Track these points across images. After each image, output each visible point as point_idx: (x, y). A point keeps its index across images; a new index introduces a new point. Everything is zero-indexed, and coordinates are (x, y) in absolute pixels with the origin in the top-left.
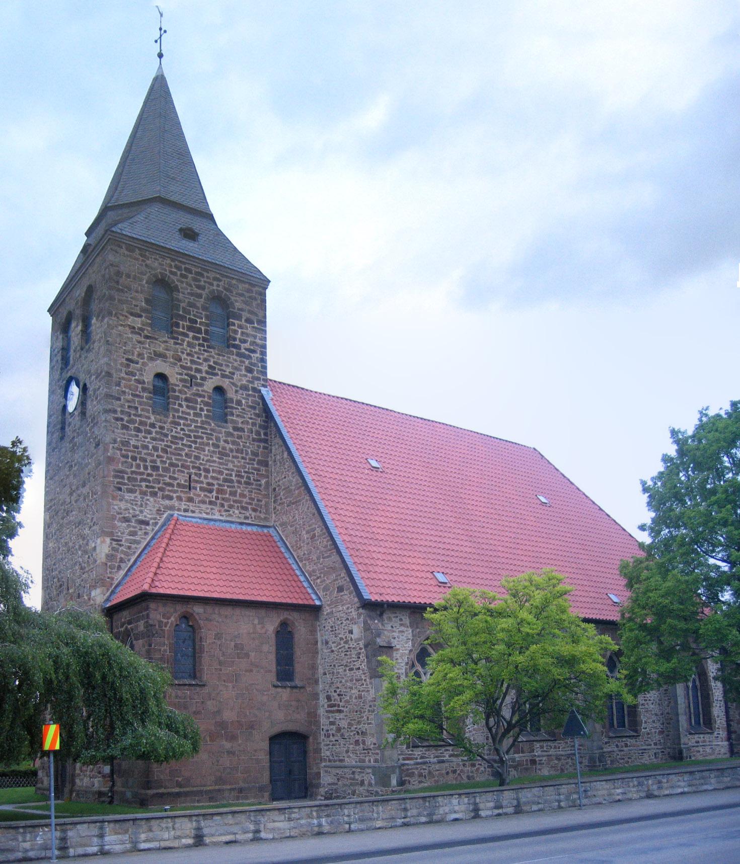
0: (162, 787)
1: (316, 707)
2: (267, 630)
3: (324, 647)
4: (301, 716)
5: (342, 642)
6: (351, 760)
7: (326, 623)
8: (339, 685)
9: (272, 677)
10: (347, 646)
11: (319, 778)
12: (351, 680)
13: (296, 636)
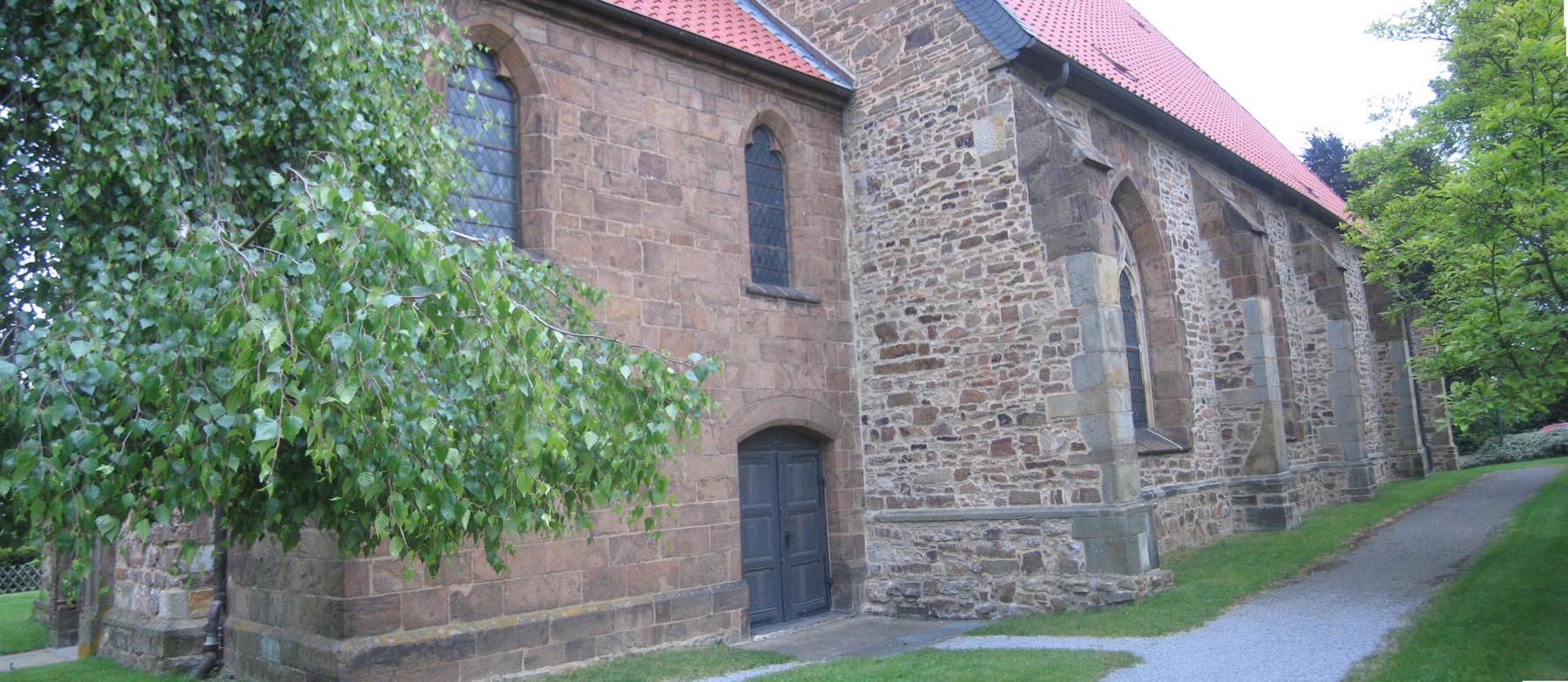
0: (395, 624)
1: (846, 358)
2: (724, 134)
3: (865, 198)
4: (815, 383)
5: (932, 174)
6: (983, 499)
7: (871, 131)
8: (923, 291)
9: (741, 267)
10: (950, 183)
11: (861, 552)
12: (974, 272)
13: (792, 165)
